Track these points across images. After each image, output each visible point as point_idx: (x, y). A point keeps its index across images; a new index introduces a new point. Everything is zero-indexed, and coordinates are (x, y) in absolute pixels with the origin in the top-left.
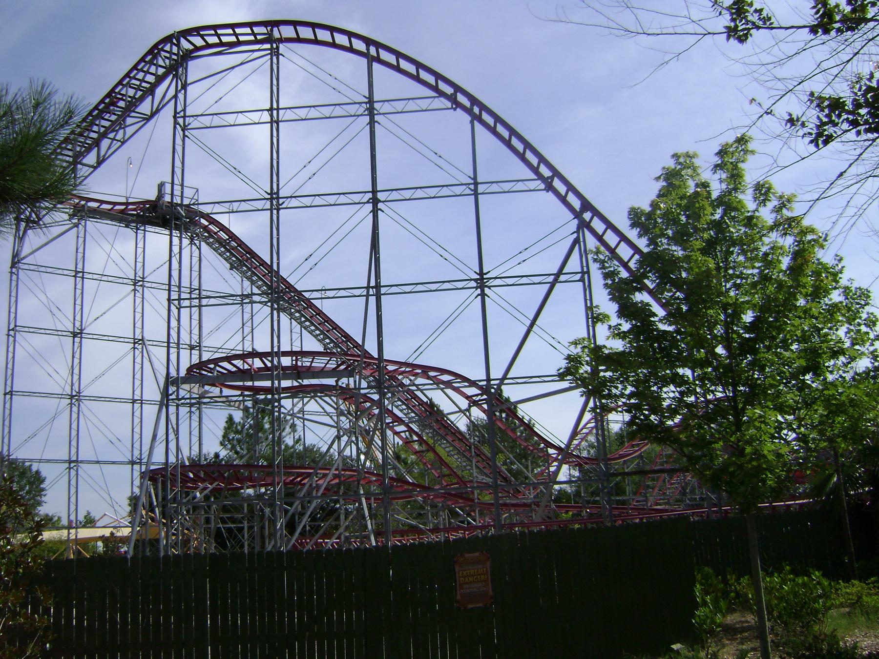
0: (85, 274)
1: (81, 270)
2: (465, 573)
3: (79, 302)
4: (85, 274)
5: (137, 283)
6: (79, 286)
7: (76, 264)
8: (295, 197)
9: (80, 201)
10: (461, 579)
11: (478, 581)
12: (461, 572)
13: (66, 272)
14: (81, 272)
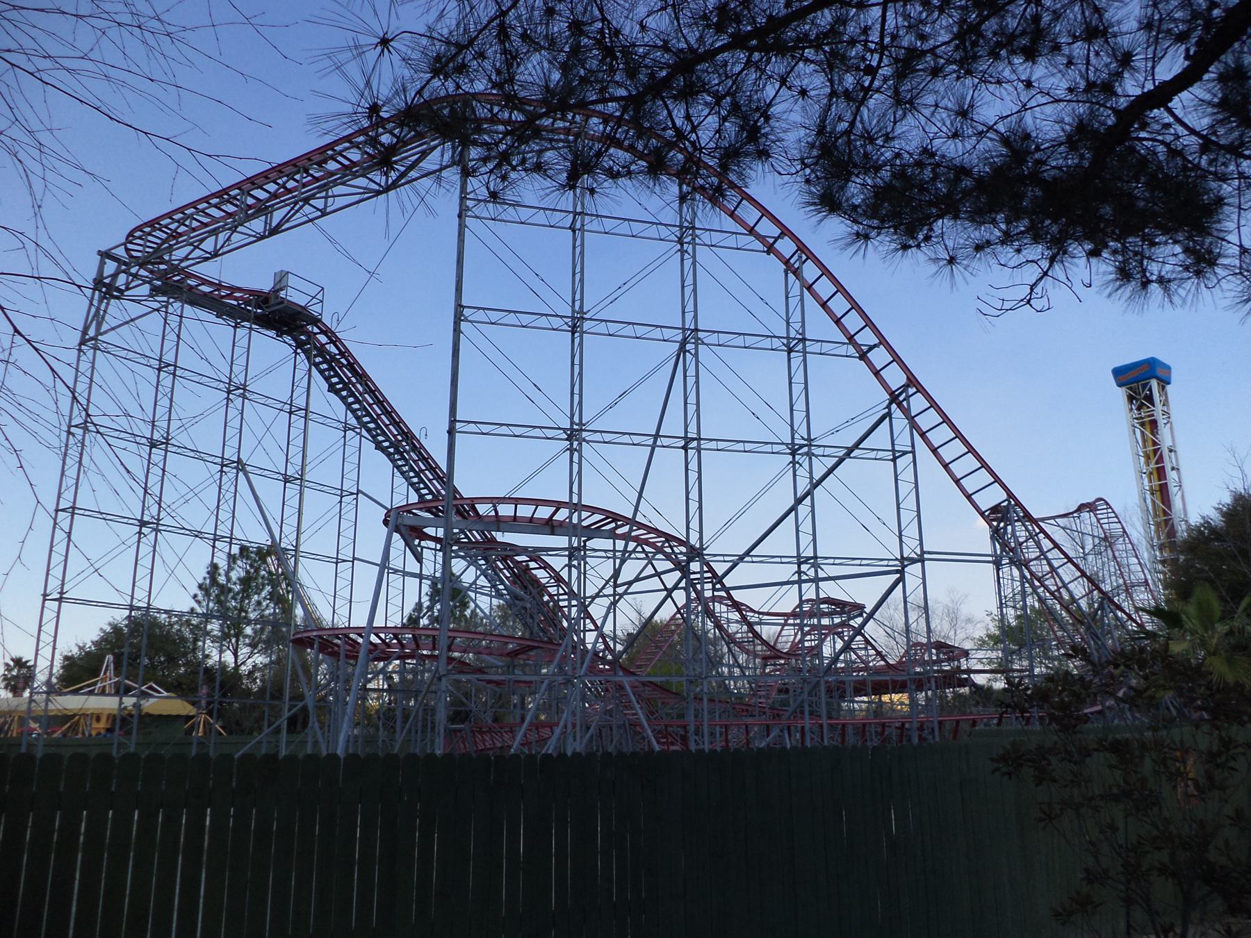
0: (702, 442)
1: (695, 436)
3: (694, 495)
5: (798, 449)
6: (693, 465)
7: (686, 426)
8: (900, 532)
9: (553, 124)
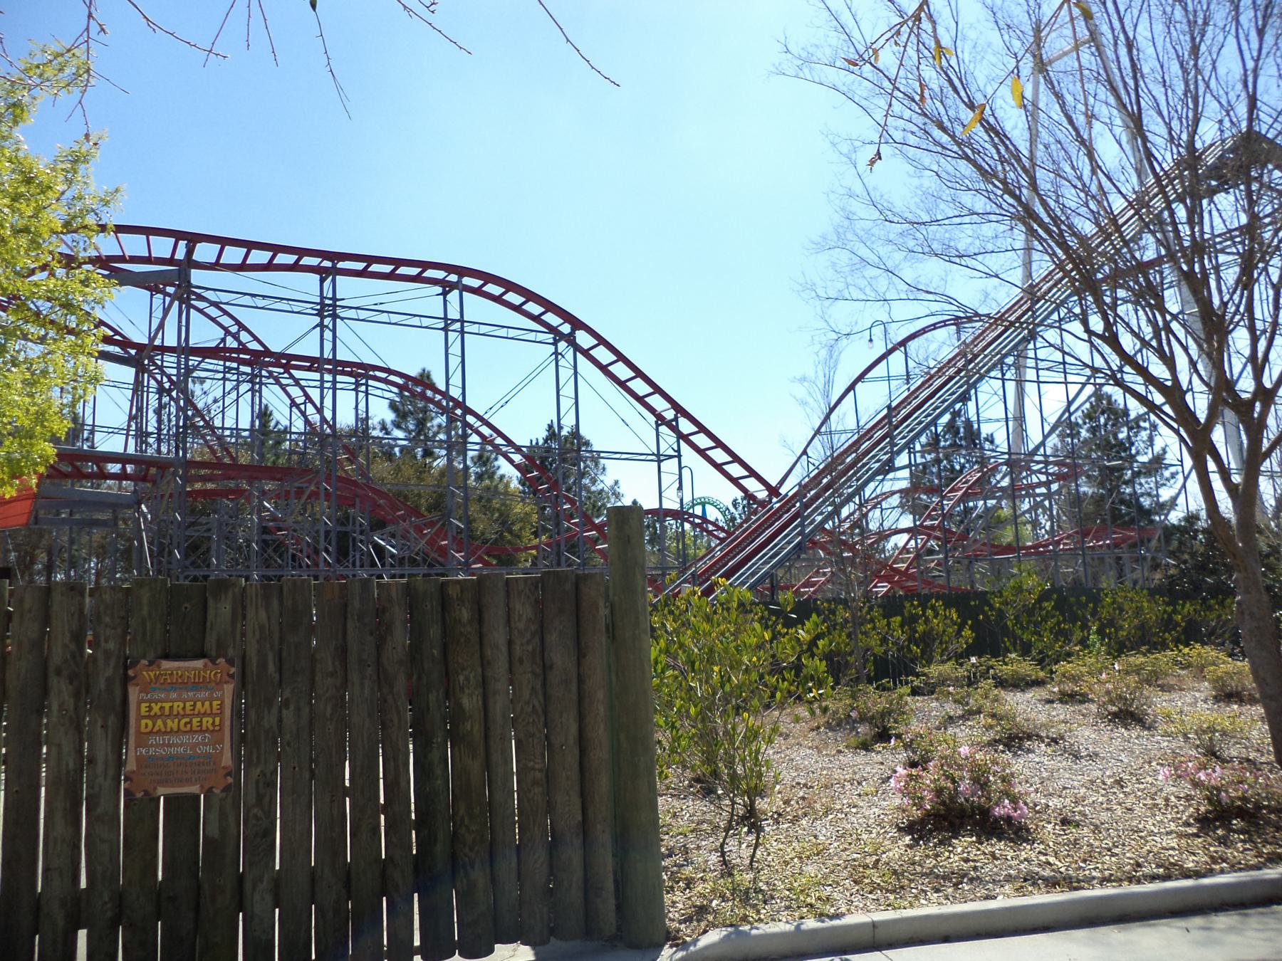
0: (466, 324)
2: (156, 708)
4: (466, 324)
10: (143, 722)
11: (191, 730)
12: (144, 705)
13: (426, 322)
14: (457, 321)
